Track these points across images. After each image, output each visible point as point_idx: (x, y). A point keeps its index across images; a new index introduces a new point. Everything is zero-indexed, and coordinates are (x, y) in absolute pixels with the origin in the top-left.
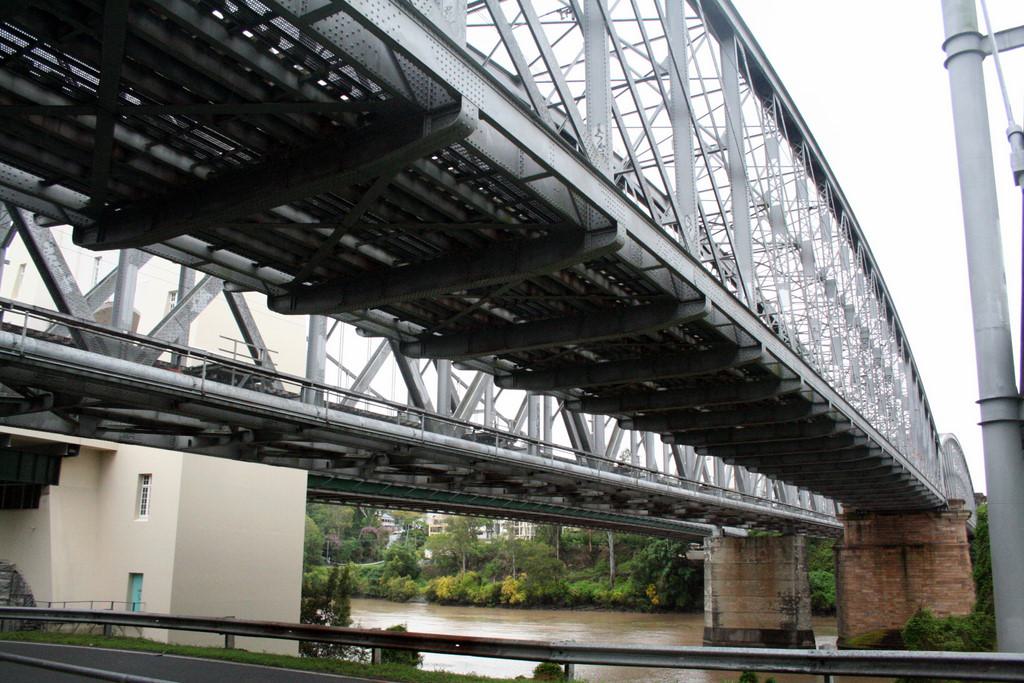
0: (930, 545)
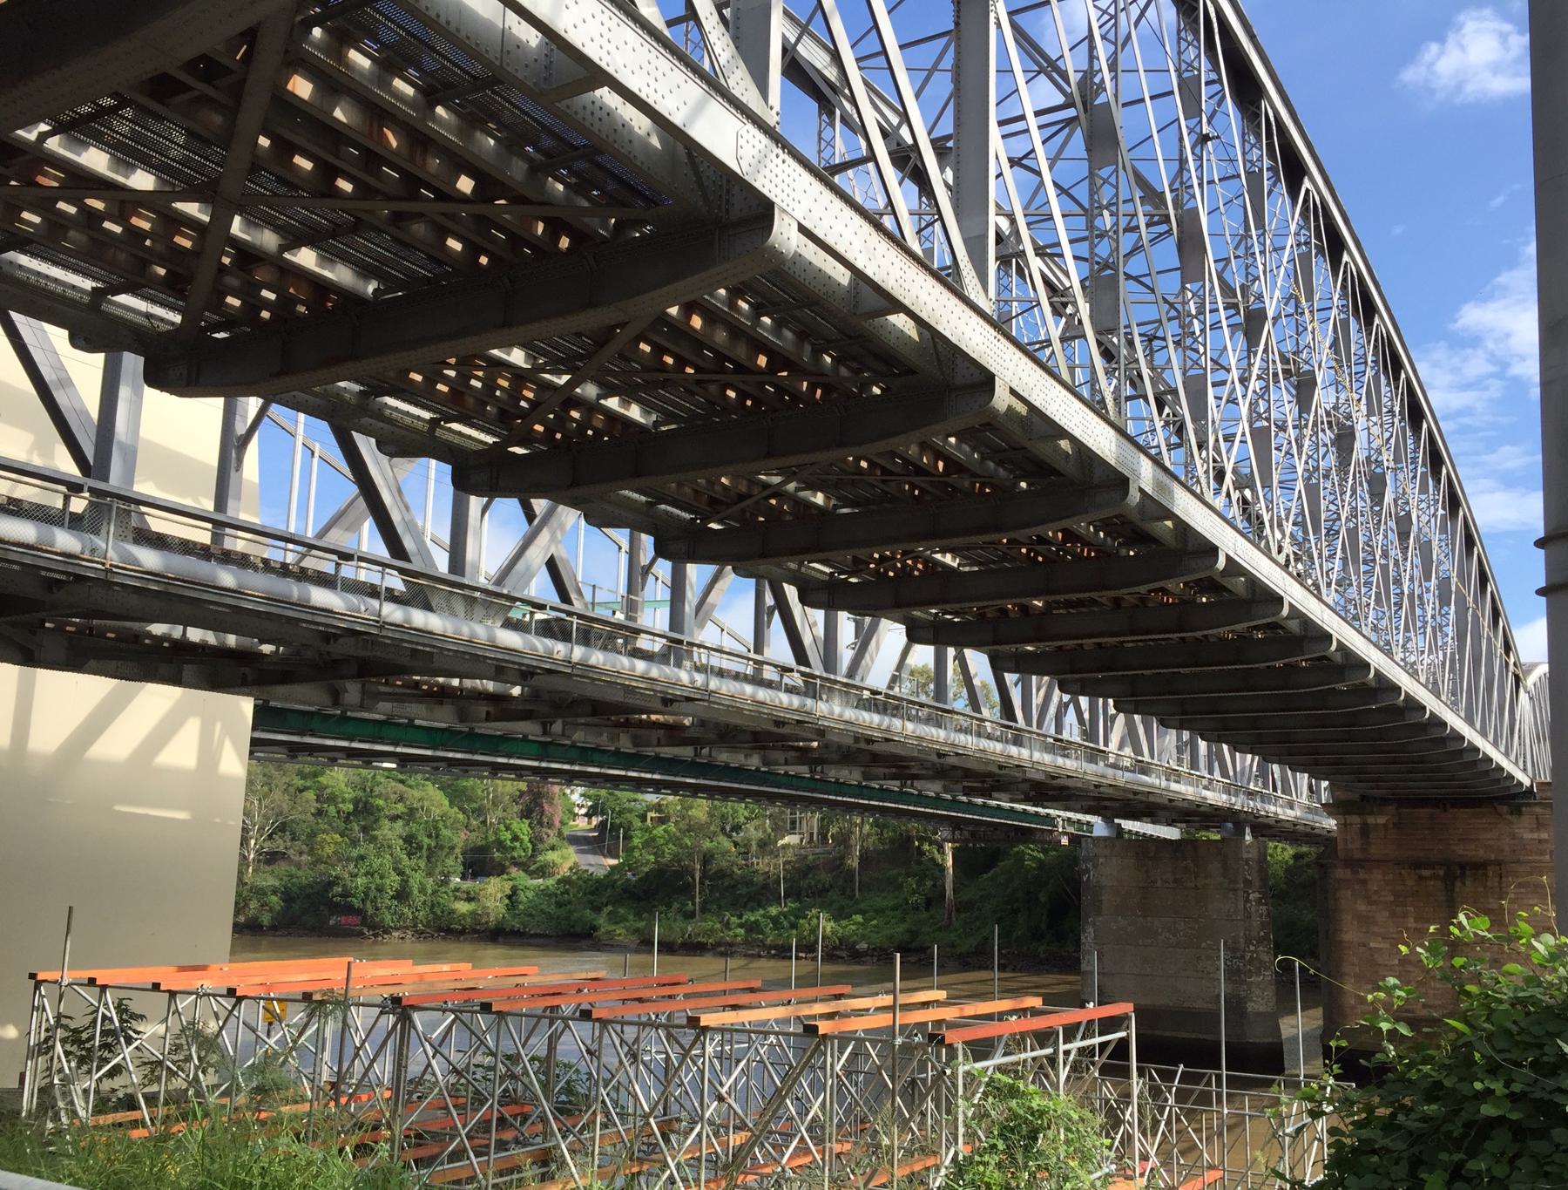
0: (1499, 863)
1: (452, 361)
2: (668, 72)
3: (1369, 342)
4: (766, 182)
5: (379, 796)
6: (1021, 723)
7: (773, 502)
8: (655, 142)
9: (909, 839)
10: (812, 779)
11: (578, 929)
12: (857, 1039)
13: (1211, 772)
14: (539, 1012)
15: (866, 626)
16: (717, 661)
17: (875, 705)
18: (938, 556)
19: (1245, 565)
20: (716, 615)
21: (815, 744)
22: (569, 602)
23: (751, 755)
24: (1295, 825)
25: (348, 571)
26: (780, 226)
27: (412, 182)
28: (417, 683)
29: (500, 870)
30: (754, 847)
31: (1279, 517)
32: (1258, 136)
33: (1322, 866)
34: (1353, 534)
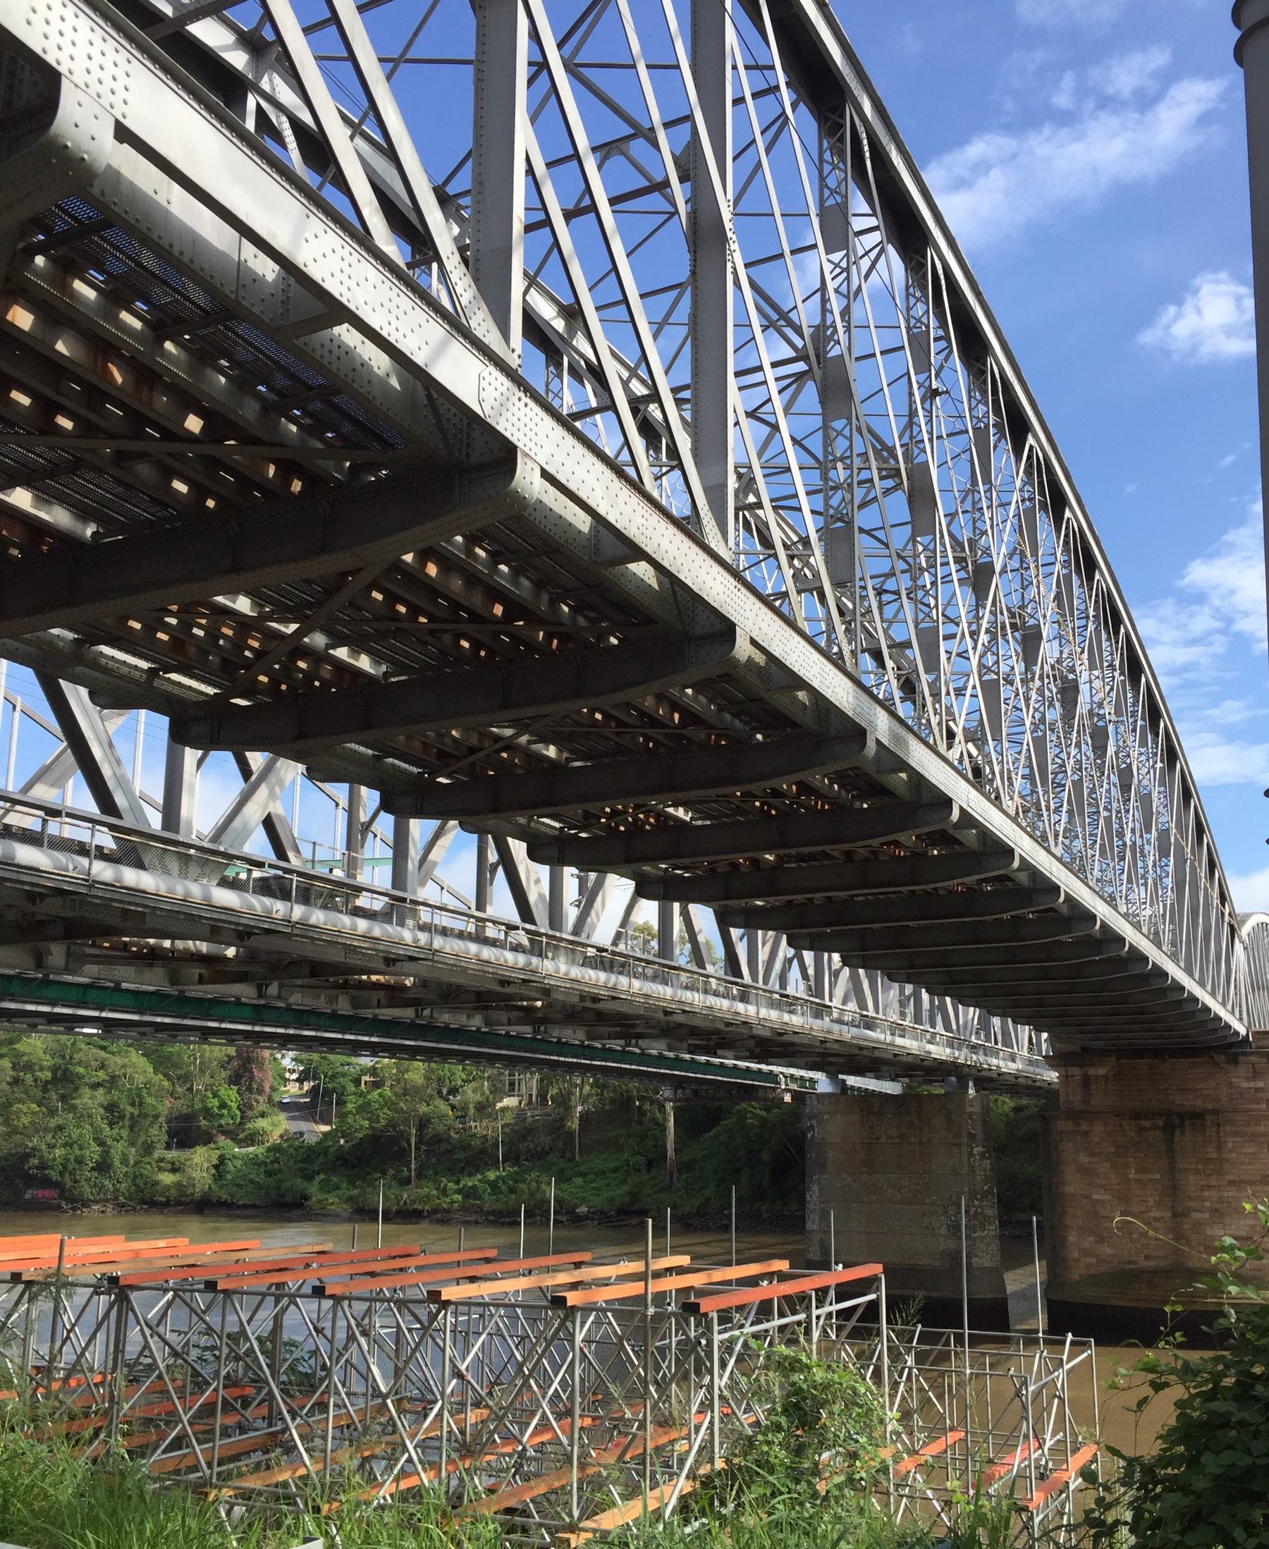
0: (1216, 1112)
1: (174, 608)
2: (409, 310)
3: (1090, 597)
4: (509, 425)
5: (80, 1063)
6: (747, 978)
7: (505, 755)
8: (394, 382)
9: (630, 1100)
10: (534, 1039)
11: (289, 1199)
12: (597, 1310)
13: (933, 1025)
14: (264, 1289)
15: (590, 885)
16: (444, 920)
17: (602, 962)
18: (671, 810)
19: (978, 817)
20: (437, 873)
21: (539, 1004)
22: (286, 859)
23: (473, 1016)
24: (1017, 1078)
25: (54, 827)
26: (523, 470)
27: (137, 420)
28: (126, 944)
29: (207, 1139)
30: (472, 1111)
31: (1009, 770)
32: (984, 392)
33: (1044, 1118)
34: (1078, 785)
